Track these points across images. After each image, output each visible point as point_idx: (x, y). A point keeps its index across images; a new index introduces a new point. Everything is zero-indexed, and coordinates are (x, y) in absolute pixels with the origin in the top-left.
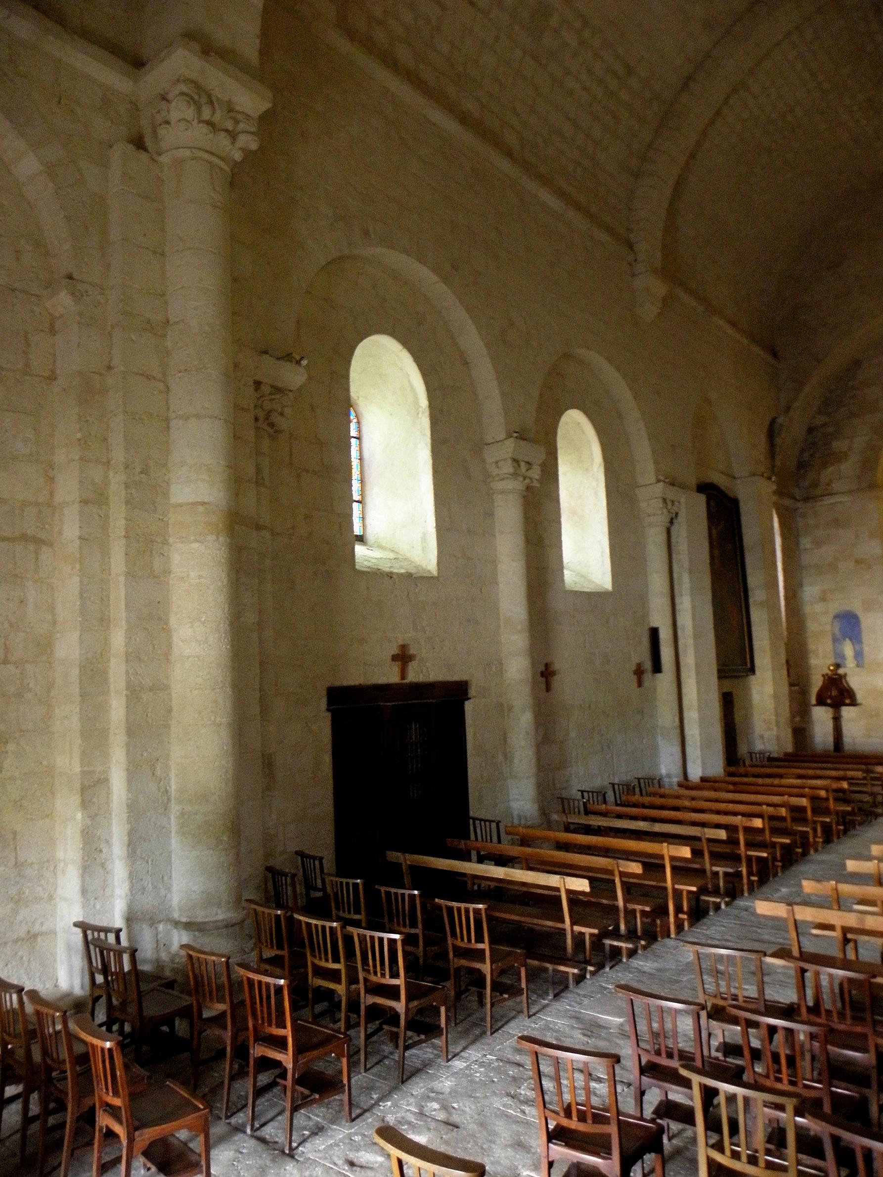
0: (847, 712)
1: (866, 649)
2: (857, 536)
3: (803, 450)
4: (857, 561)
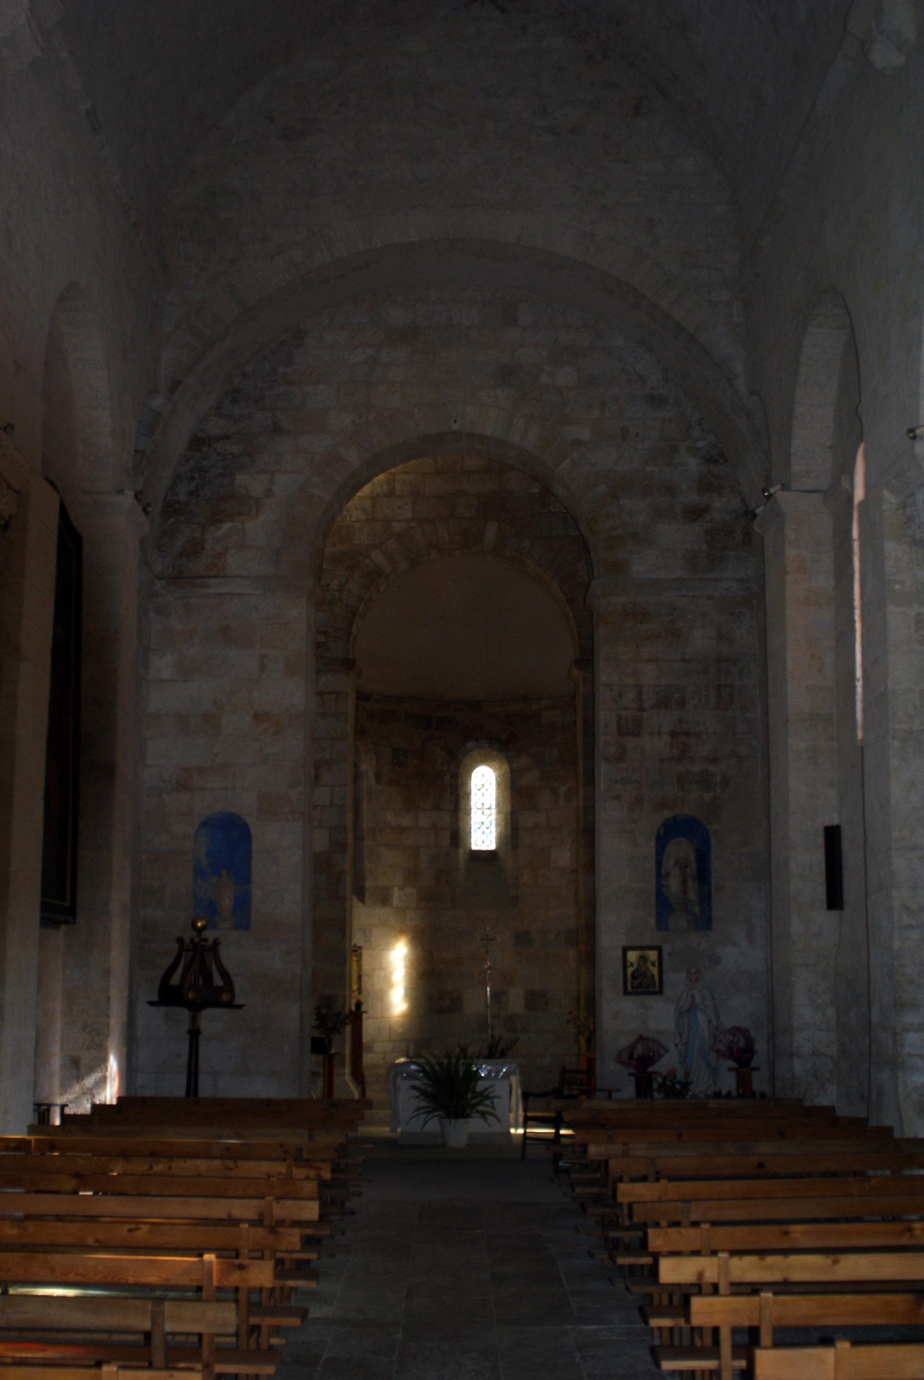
0: (213, 1020)
1: (257, 893)
2: (263, 668)
3: (177, 479)
4: (256, 716)
